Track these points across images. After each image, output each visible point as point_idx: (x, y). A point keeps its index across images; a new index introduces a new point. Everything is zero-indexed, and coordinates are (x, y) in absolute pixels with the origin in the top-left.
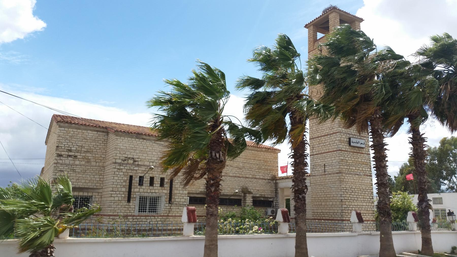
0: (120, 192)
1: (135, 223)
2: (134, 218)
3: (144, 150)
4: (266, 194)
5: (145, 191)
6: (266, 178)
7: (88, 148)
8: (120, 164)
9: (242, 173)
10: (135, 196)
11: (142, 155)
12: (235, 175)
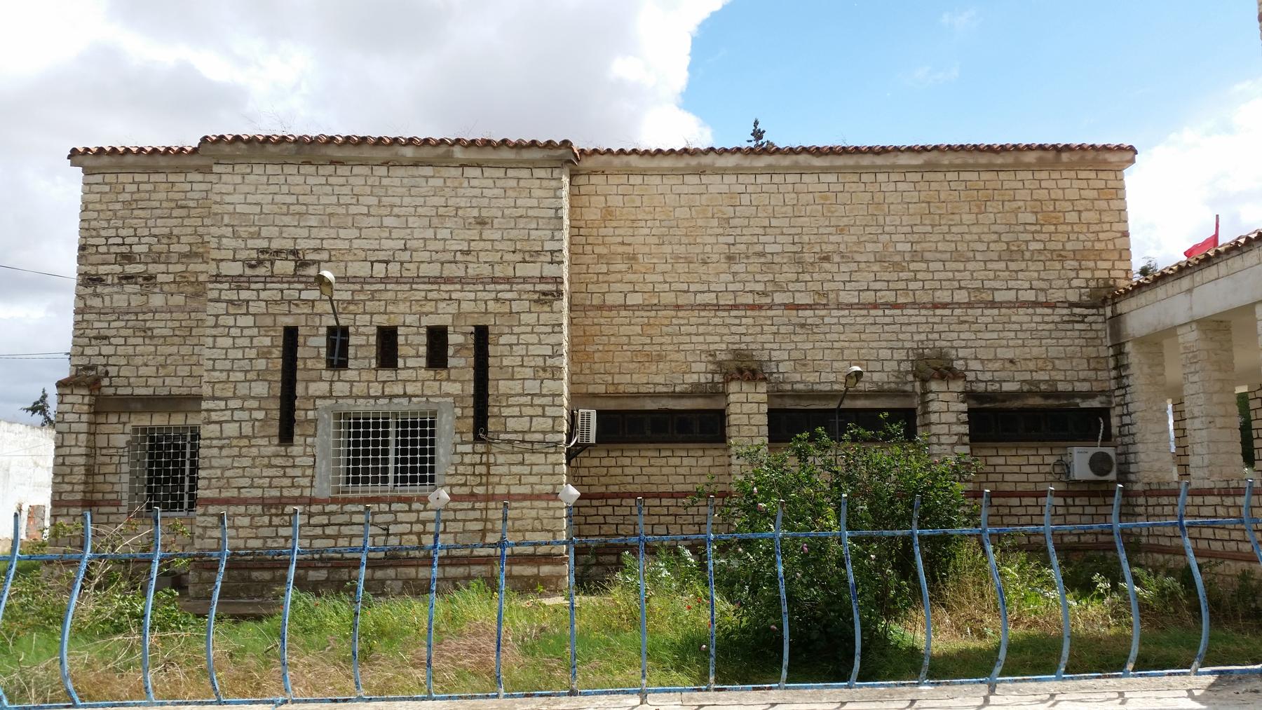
0: (244, 398)
1: (319, 531)
2: (314, 508)
3: (342, 210)
4: (1060, 376)
5: (359, 389)
6: (1057, 296)
7: (191, 239)
8: (237, 282)
9: (912, 285)
10: (311, 414)
11: (333, 233)
12: (868, 297)
